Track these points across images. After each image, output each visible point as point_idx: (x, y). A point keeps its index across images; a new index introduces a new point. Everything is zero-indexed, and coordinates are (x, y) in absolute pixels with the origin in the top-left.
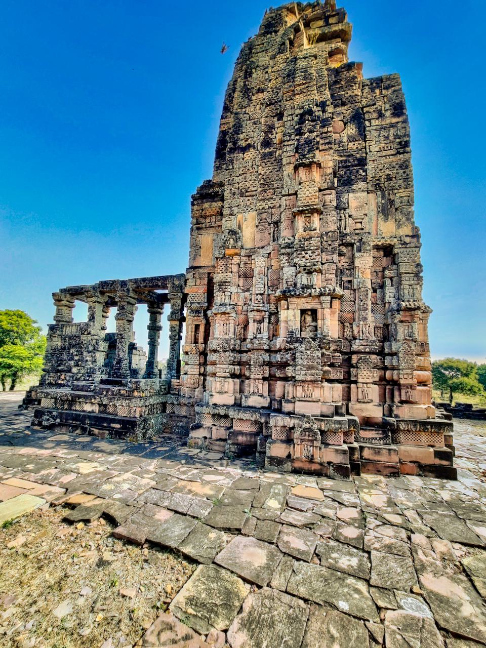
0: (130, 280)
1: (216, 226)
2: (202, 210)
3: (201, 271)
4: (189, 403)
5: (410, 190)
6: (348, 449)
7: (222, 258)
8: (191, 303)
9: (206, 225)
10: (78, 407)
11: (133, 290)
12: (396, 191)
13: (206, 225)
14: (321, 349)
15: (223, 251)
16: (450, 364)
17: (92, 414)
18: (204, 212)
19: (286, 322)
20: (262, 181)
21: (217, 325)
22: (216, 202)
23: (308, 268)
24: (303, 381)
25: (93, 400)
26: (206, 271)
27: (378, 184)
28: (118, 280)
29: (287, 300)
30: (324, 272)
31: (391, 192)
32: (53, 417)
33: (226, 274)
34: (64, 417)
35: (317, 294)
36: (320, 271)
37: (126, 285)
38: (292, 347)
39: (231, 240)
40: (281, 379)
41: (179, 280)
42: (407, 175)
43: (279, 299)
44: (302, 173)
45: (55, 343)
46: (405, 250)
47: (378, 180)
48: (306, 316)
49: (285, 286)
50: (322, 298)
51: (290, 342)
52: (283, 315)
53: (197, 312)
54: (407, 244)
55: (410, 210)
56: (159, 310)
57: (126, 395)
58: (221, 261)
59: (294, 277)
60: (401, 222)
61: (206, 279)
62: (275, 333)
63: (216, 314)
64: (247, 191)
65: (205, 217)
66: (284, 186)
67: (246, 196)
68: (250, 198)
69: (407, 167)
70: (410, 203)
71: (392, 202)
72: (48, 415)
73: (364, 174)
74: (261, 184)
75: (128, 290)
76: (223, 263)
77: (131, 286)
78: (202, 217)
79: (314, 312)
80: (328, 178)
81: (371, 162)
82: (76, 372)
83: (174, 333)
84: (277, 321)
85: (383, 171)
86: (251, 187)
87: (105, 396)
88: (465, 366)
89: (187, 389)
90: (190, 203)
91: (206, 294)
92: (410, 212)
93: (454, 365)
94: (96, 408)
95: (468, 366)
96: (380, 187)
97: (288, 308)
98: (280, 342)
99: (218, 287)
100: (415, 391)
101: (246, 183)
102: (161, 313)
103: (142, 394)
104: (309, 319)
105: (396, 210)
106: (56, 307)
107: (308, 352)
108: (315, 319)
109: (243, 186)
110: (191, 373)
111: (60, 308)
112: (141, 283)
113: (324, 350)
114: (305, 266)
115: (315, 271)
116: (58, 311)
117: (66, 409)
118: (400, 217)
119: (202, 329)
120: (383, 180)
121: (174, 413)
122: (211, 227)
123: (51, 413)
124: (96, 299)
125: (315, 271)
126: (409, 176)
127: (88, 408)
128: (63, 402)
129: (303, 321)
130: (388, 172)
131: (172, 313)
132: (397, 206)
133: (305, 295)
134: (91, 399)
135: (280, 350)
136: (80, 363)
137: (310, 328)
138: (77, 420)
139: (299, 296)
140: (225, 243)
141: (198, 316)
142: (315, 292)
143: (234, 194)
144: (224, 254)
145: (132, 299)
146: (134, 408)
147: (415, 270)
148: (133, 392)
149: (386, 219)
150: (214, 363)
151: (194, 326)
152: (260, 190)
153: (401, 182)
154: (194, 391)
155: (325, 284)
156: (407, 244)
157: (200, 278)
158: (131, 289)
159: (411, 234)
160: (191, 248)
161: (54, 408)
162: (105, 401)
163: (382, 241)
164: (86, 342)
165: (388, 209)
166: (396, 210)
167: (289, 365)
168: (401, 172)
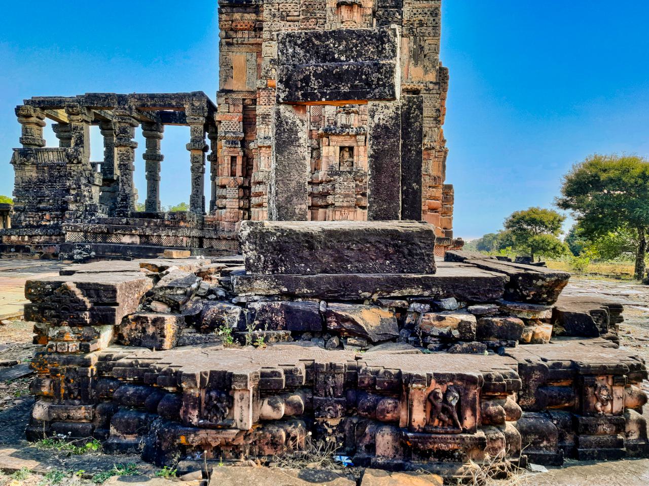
0: (133, 96)
1: (250, 44)
2: (232, 21)
3: (234, 96)
4: (229, 237)
5: (437, 38)
6: (426, 376)
7: (264, 89)
8: (225, 133)
9: (237, 41)
10: (114, 240)
11: (136, 109)
12: (426, 38)
13: (237, 41)
14: (356, 181)
15: (265, 81)
16: (534, 216)
17: (134, 246)
18: (234, 24)
19: (327, 157)
20: (304, 8)
21: (262, 158)
22: (249, 13)
23: (347, 109)
24: (342, 207)
25: (134, 231)
26: (240, 96)
27: (411, 28)
28: (114, 94)
29: (328, 138)
30: (360, 113)
31: (422, 38)
32: (86, 250)
33: (269, 107)
34: (101, 249)
35: (354, 133)
36: (357, 113)
37: (126, 102)
38: (332, 179)
39: (274, 70)
40: (321, 207)
41: (200, 100)
42: (436, 23)
43: (321, 136)
44: (344, 11)
45: (28, 174)
46: (428, 95)
47: (412, 24)
48: (345, 153)
49: (327, 123)
50: (358, 137)
51: (331, 175)
52: (325, 150)
53: (233, 143)
54: (431, 90)
55: (436, 58)
56: (159, 133)
57: (171, 225)
58: (264, 92)
59: (334, 116)
60: (428, 69)
61: (241, 106)
62: (317, 167)
63: (260, 147)
64: (288, 16)
65: (236, 31)
66: (327, 21)
67: (287, 21)
68: (291, 23)
69: (437, 15)
70: (436, 52)
71: (422, 48)
72: (79, 249)
73: (399, 17)
74: (303, 10)
75: (130, 108)
76: (266, 95)
77: (133, 103)
78: (232, 30)
79: (351, 149)
80: (367, 19)
81: (407, 5)
82: (74, 209)
83: (197, 165)
84: (319, 157)
85: (416, 16)
86: (292, 10)
87: (147, 227)
88: (551, 218)
89: (226, 223)
90: (217, 10)
91: (241, 123)
92: (436, 59)
93: (538, 218)
94: (137, 240)
95: (555, 218)
96: (413, 32)
97: (329, 145)
98: (322, 175)
99: (261, 119)
100: (427, 216)
101: (287, 5)
102: (160, 138)
103: (188, 225)
104: (346, 155)
105: (425, 56)
106: (20, 125)
107: (345, 183)
108: (351, 156)
109: (284, 8)
110: (230, 207)
111: (28, 126)
112: (148, 101)
113: (358, 182)
114: (345, 107)
115: (353, 112)
116: (25, 131)
117: (100, 242)
118: (428, 64)
119: (239, 161)
120: (416, 25)
121: (212, 247)
122: (243, 44)
123: (83, 246)
124: (84, 117)
125: (353, 112)
126: (437, 25)
127: (126, 240)
128: (95, 234)
129: (341, 157)
130: (420, 17)
131: (192, 141)
132: (426, 53)
133: (344, 134)
134: (131, 231)
135: (321, 183)
136: (78, 198)
137: (347, 163)
138: (115, 252)
139: (338, 135)
140: (267, 73)
141: (235, 147)
142: (352, 131)
143: (274, 16)
144: (267, 85)
145: (135, 121)
146: (181, 238)
147: (435, 114)
148: (179, 222)
149: (416, 64)
150: (259, 195)
151: (230, 158)
152: (302, 17)
153: (430, 29)
154: (234, 225)
155: (361, 124)
156: (431, 90)
157: (234, 105)
158: (134, 107)
159: (434, 81)
160: (220, 67)
161: (85, 242)
162: (148, 232)
163: (412, 85)
164: (75, 173)
165: (418, 55)
166: (425, 56)
167: (330, 194)
168: (432, 19)
